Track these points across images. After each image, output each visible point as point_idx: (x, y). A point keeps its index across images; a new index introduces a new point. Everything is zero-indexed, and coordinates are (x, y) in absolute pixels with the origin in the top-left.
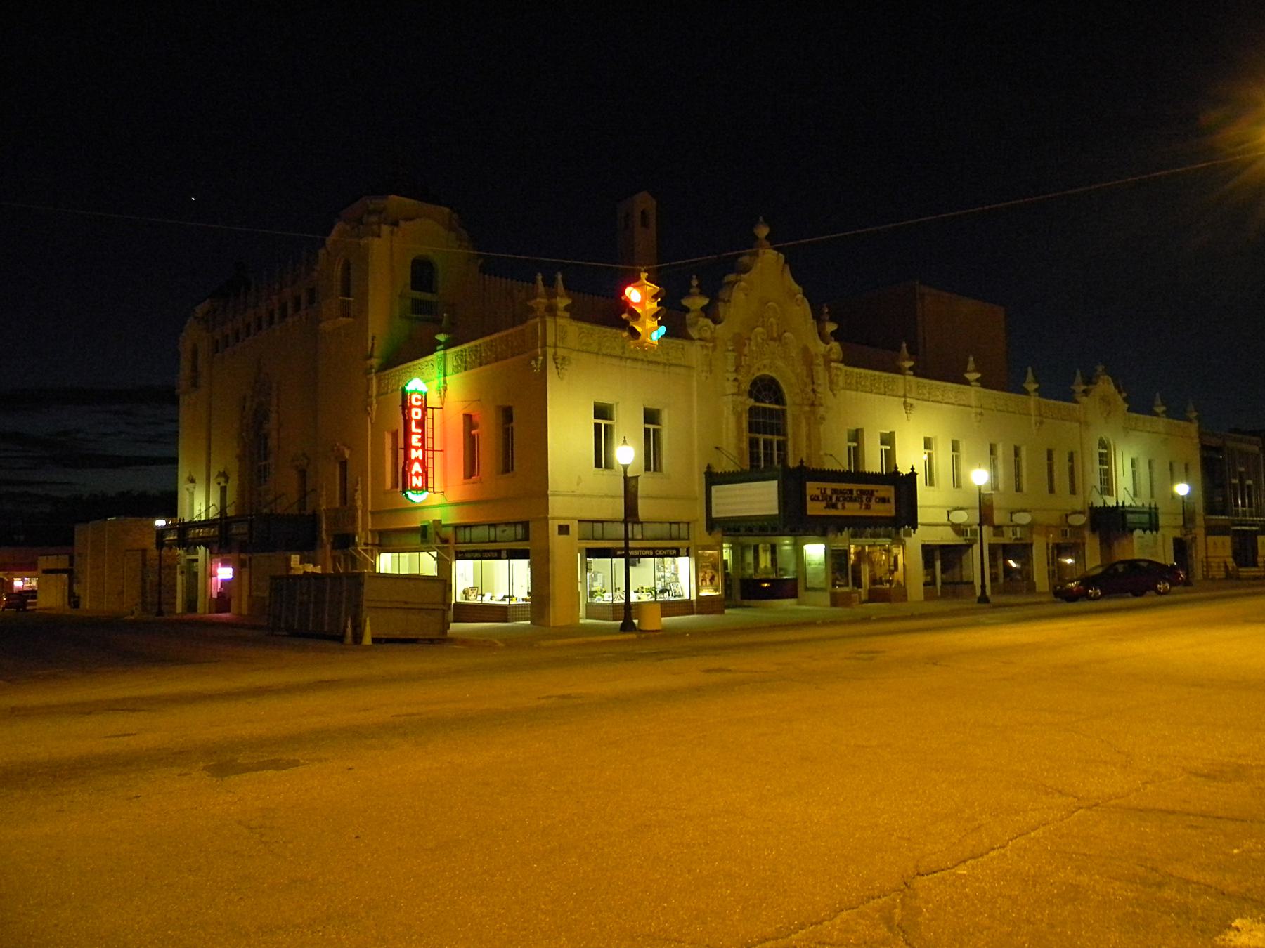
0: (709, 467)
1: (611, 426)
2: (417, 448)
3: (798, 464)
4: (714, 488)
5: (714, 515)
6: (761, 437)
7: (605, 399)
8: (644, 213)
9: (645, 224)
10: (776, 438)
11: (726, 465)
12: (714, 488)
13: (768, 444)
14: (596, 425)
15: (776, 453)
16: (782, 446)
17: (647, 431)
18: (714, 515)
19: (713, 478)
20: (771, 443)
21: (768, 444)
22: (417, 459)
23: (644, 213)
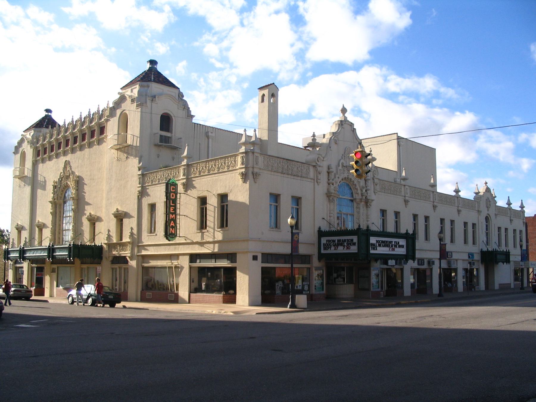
0: (320, 228)
22: (172, 219)
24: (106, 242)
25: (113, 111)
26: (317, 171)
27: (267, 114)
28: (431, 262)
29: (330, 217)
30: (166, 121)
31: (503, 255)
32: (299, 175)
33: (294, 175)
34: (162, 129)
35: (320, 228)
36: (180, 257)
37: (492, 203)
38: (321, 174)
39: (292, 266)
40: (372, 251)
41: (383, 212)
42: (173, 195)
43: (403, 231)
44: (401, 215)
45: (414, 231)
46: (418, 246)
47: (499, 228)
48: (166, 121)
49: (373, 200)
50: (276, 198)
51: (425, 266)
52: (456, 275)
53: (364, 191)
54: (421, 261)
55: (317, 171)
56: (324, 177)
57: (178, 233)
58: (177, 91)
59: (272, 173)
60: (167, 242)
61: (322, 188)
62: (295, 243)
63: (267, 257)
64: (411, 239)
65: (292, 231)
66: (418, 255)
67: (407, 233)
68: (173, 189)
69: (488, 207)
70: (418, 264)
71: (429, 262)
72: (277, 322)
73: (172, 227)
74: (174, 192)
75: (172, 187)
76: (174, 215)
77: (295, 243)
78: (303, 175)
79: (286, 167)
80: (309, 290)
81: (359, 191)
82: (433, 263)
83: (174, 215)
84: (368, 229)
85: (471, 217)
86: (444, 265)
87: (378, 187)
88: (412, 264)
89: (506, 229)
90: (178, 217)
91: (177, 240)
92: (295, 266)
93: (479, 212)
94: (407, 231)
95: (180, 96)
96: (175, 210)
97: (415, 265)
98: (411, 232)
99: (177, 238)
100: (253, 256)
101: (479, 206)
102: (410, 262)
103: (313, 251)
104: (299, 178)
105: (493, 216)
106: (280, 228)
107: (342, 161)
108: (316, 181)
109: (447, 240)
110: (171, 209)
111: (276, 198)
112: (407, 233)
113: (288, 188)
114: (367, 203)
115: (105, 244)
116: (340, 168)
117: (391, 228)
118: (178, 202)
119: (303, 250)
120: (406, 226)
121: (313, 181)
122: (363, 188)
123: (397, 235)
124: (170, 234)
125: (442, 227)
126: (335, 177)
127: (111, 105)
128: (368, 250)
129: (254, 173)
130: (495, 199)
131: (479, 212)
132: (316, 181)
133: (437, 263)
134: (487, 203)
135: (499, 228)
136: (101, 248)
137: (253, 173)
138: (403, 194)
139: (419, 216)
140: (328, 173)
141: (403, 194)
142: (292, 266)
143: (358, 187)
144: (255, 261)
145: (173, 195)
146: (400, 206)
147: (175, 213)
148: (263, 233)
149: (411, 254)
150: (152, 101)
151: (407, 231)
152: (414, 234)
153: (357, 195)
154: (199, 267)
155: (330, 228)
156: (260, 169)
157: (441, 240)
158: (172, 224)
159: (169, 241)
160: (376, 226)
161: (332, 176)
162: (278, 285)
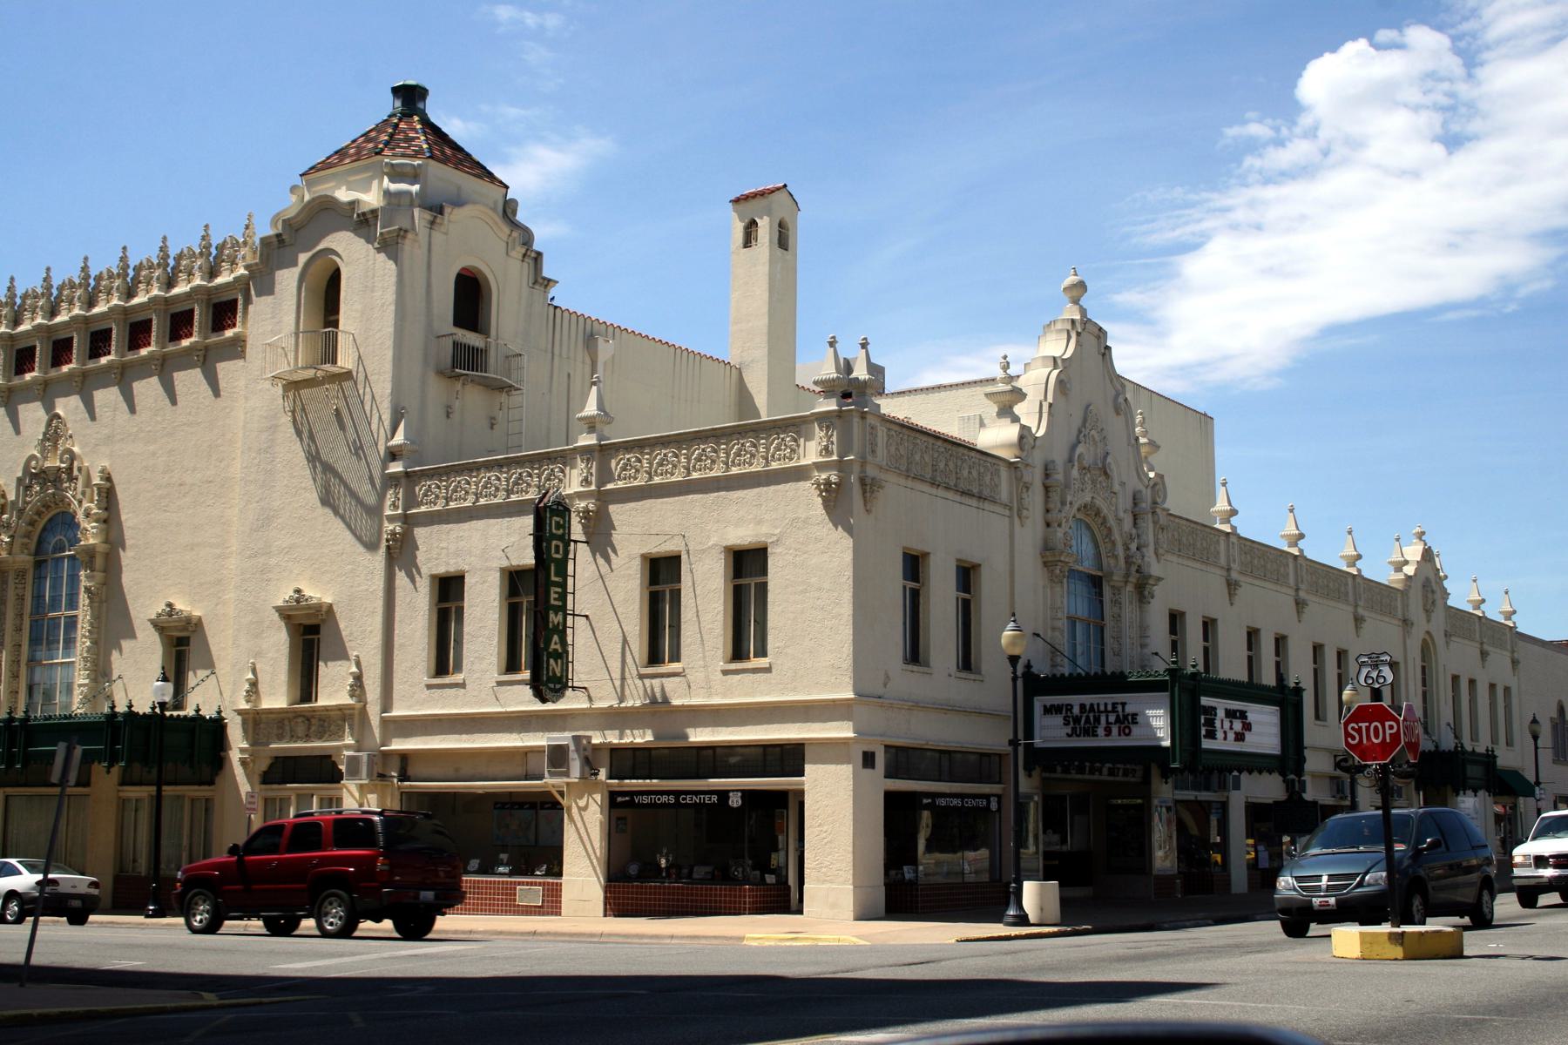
24: (244, 706)
25: (276, 250)
26: (1019, 479)
27: (765, 286)
29: (1053, 629)
30: (471, 297)
32: (975, 491)
33: (963, 493)
34: (458, 322)
37: (1438, 596)
40: (1207, 744)
41: (1176, 620)
42: (557, 547)
44: (1221, 629)
47: (1455, 678)
48: (471, 297)
49: (1159, 579)
50: (914, 565)
53: (1133, 546)
55: (1019, 479)
56: (1035, 499)
58: (497, 192)
59: (910, 483)
60: (538, 706)
61: (1029, 535)
63: (902, 760)
68: (558, 526)
69: (1428, 612)
72: (979, 977)
78: (986, 493)
79: (942, 465)
85: (1382, 634)
89: (1472, 682)
90: (570, 618)
91: (571, 702)
92: (168, 790)
93: (1406, 623)
95: (509, 211)
96: (563, 597)
99: (569, 692)
100: (873, 754)
101: (1406, 606)
104: (974, 502)
105: (1440, 640)
106: (927, 665)
107: (1080, 449)
108: (1017, 511)
110: (553, 596)
111: (914, 565)
113: (950, 530)
114: (1143, 587)
115: (240, 712)
116: (1075, 473)
121: (1007, 512)
122: (1132, 539)
126: (1063, 503)
127: (264, 229)
129: (868, 481)
130: (1446, 583)
131: (1406, 623)
132: (1017, 511)
134: (1425, 597)
135: (1455, 678)
136: (217, 727)
137: (862, 482)
138: (1223, 561)
140: (1047, 488)
141: (1223, 561)
142: (159, 791)
143: (1116, 536)
144: (869, 771)
145: (557, 547)
146: (1217, 605)
150: (432, 223)
153: (1112, 561)
155: (1054, 666)
158: (555, 645)
159: (544, 701)
161: (1055, 497)
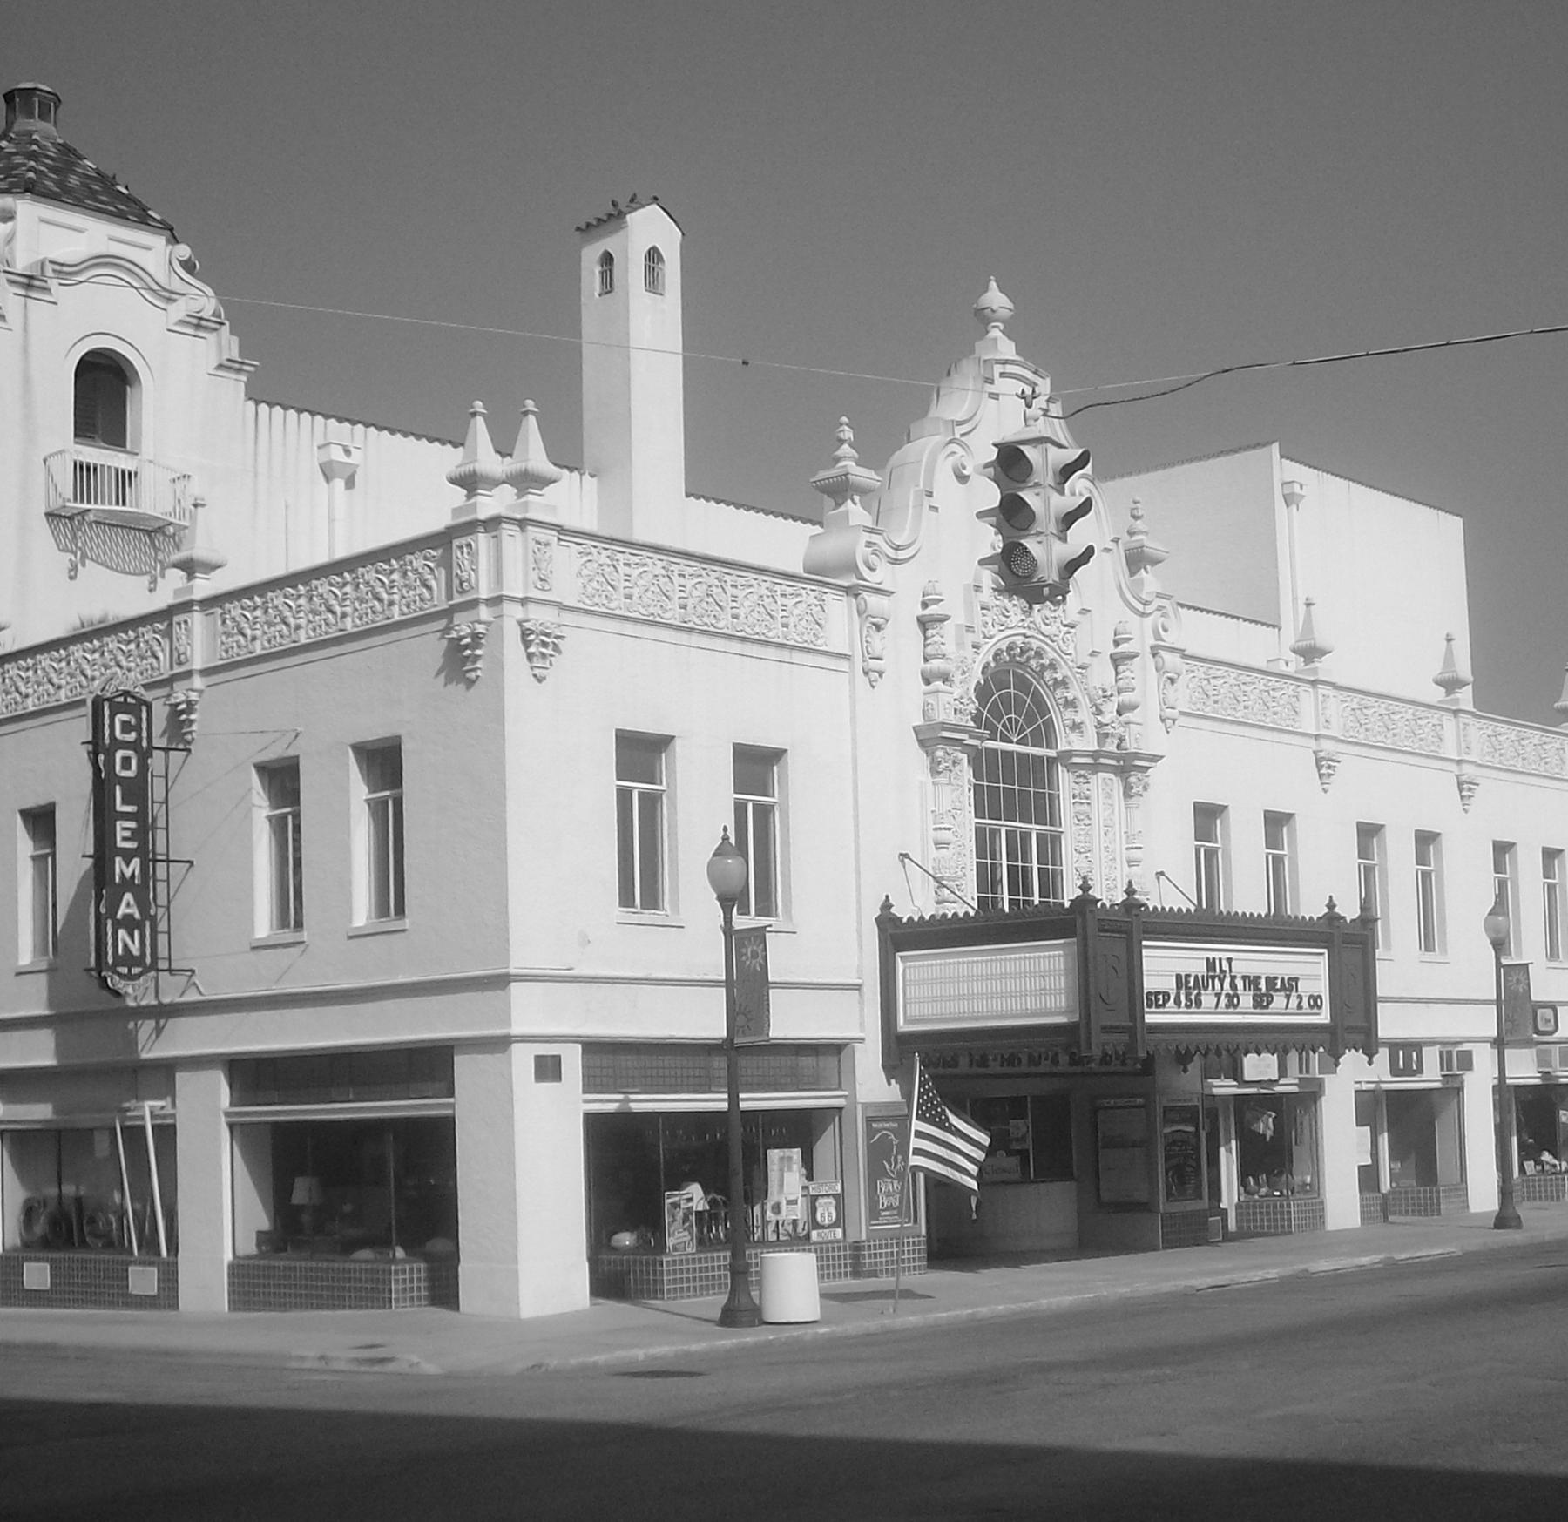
0: (887, 906)
1: (1496, 872)
2: (128, 856)
3: (1120, 897)
4: (903, 965)
5: (902, 1026)
6: (1004, 826)
7: (374, 730)
8: (653, 256)
9: (653, 281)
10: (1034, 828)
11: (917, 904)
12: (903, 965)
13: (1018, 845)
14: (980, 831)
15: (1005, 863)
16: (1050, 845)
17: (624, 797)
18: (902, 1026)
19: (899, 936)
20: (1026, 836)
21: (1018, 845)
22: (127, 884)
23: (653, 256)
28: (1457, 1059)
31: (7, 192)
35: (887, 906)
36: (181, 1078)
38: (889, 629)
39: (733, 1100)
40: (1151, 1018)
41: (1207, 816)
42: (126, 763)
43: (1310, 908)
45: (1366, 905)
46: (1387, 980)
51: (1431, 1076)
52: (36, 1298)
53: (1110, 714)
54: (1407, 1053)
57: (162, 951)
62: (747, 985)
64: (1349, 944)
65: (728, 919)
66: (1391, 1024)
67: (1332, 918)
68: (126, 727)
70: (1395, 1071)
71: (1446, 1060)
73: (129, 924)
74: (134, 745)
75: (120, 717)
76: (136, 862)
77: (747, 985)
80: (840, 1222)
81: (1084, 714)
82: (1466, 1061)
83: (136, 862)
84: (1131, 905)
86: (1524, 1068)
87: (1182, 696)
88: (1351, 1076)
94: (1331, 905)
96: (143, 831)
97: (1376, 1072)
98: (1350, 910)
102: (1352, 1060)
103: (855, 1022)
109: (1530, 946)
112: (1332, 918)
117: (1247, 896)
118: (159, 794)
119: (789, 1020)
120: (1325, 883)
123: (1276, 930)
124: (118, 960)
125: (1502, 884)
128: (1135, 1013)
133: (1484, 1058)
139: (1389, 834)
142: (733, 1100)
145: (126, 763)
147: (144, 852)
148: (586, 941)
149: (1353, 1023)
151: (1331, 905)
152: (1367, 920)
153: (1074, 736)
154: (276, 1124)
156: (562, 607)
157: (1499, 945)
160: (1173, 893)
162: (676, 1205)
